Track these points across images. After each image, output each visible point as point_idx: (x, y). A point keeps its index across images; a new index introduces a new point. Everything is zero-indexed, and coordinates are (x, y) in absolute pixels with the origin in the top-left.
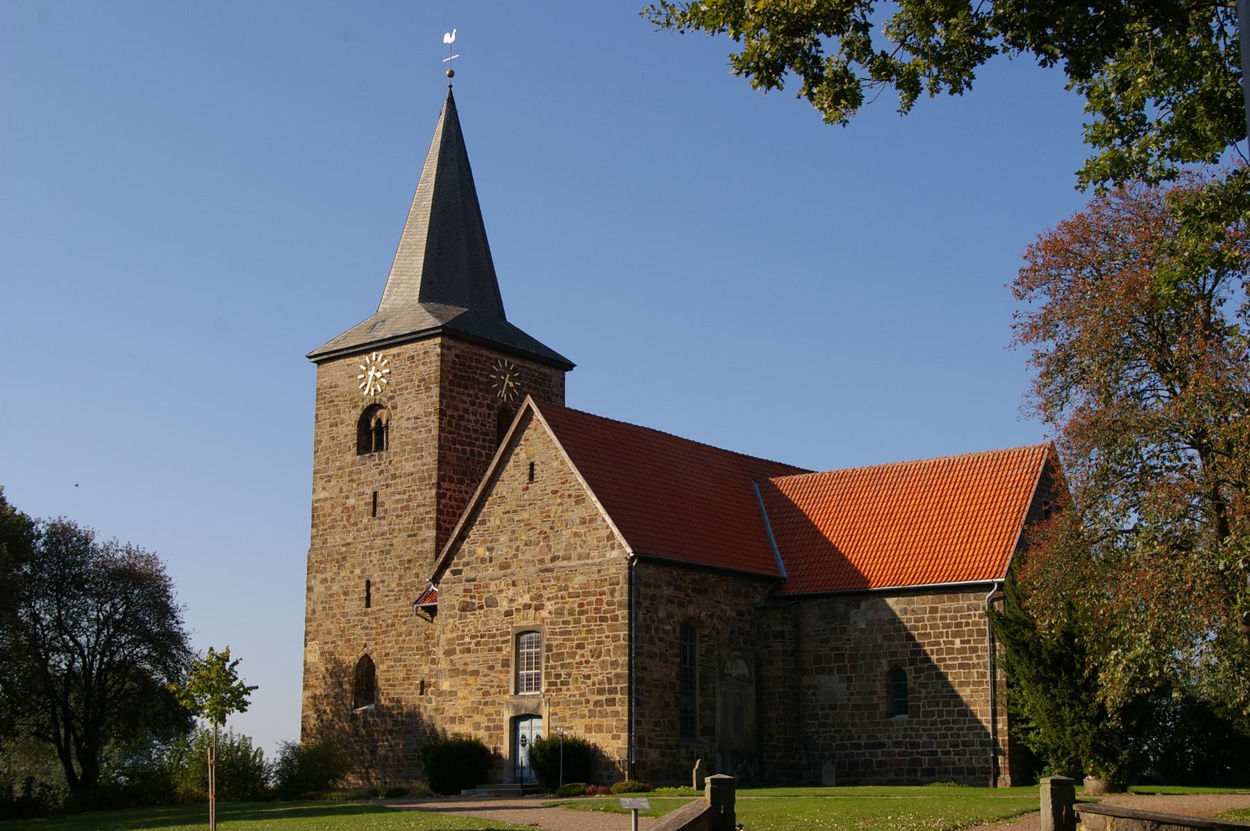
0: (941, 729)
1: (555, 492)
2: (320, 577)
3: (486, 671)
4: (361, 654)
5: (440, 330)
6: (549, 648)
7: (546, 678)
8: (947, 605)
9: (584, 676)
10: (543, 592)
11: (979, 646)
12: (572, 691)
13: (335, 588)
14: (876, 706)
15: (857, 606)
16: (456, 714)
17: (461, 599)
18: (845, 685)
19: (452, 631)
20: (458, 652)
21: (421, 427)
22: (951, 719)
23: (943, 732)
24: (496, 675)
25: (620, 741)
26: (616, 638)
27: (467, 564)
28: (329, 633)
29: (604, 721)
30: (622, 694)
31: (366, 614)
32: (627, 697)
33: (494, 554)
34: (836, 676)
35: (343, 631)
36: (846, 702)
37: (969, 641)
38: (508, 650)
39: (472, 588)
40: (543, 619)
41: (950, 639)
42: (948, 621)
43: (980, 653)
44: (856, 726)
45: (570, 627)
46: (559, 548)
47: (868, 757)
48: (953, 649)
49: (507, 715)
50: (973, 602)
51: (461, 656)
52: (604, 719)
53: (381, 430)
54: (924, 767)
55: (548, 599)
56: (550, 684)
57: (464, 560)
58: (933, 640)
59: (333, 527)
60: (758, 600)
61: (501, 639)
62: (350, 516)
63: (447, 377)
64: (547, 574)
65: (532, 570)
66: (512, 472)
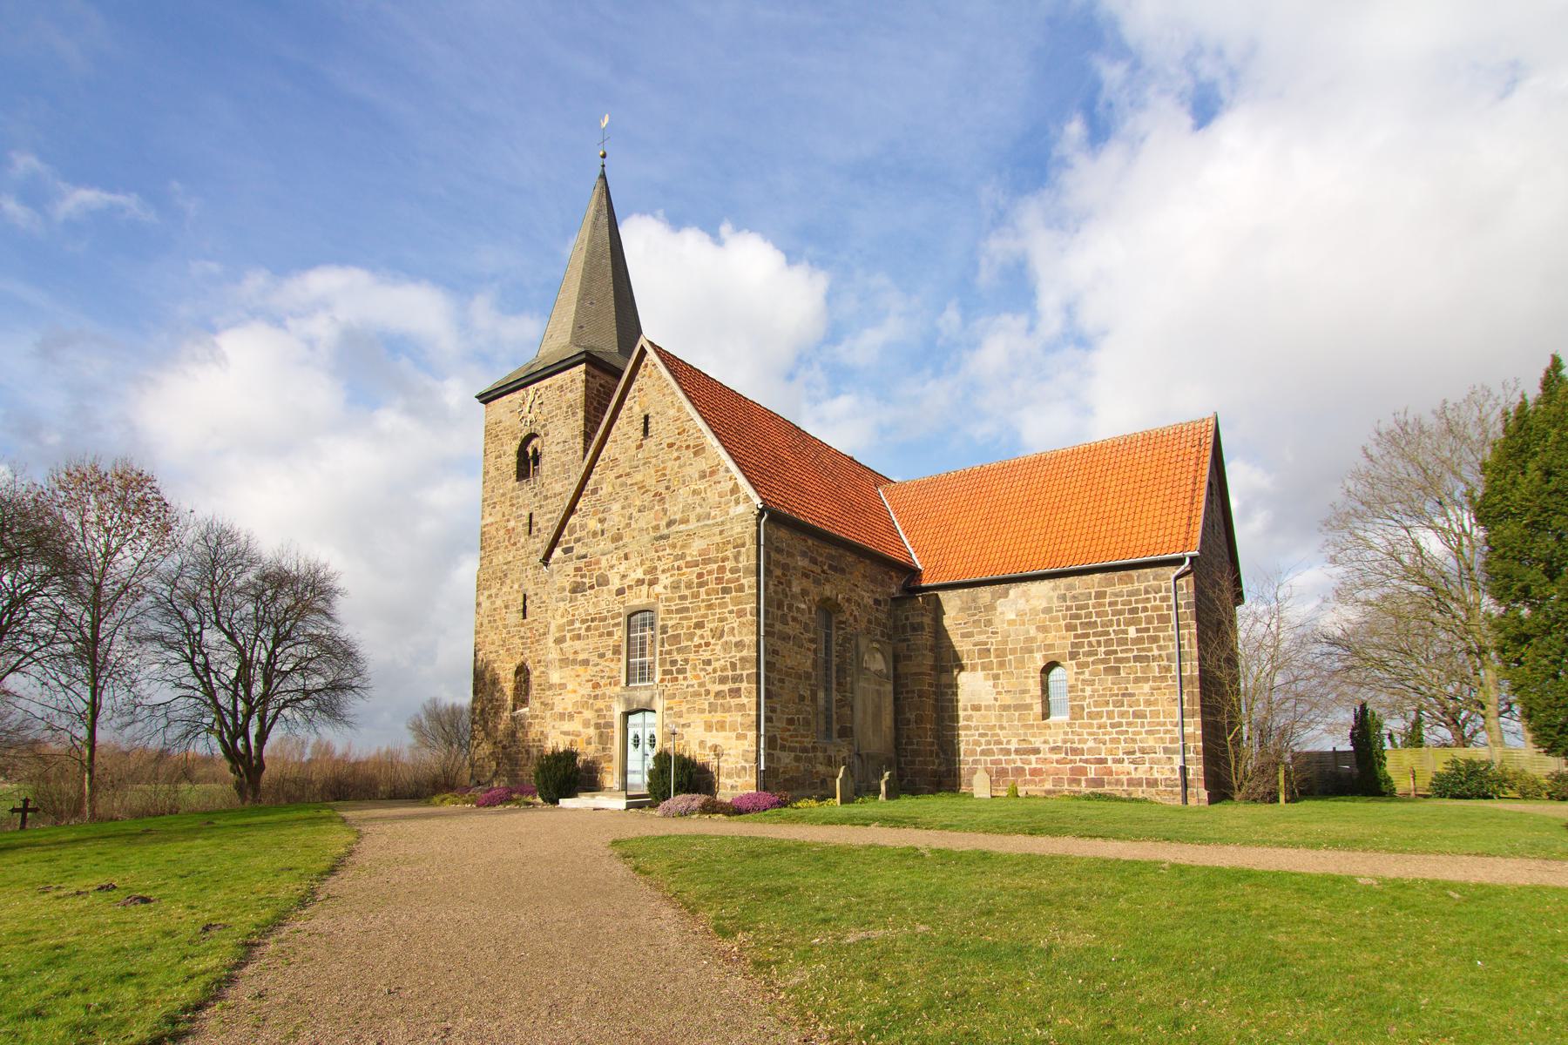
0: (1111, 733)
1: (671, 445)
2: (486, 593)
3: (596, 659)
4: (518, 662)
5: (583, 356)
6: (664, 631)
7: (661, 665)
8: (1118, 588)
9: (703, 661)
10: (657, 563)
11: (1161, 634)
12: (691, 679)
13: (499, 603)
14: (1028, 707)
15: (1006, 595)
16: (565, 709)
17: (573, 579)
18: (991, 683)
19: (562, 616)
20: (568, 639)
21: (569, 449)
22: (1124, 721)
23: (1115, 736)
24: (607, 664)
25: (746, 743)
26: (741, 614)
27: (578, 540)
28: (493, 644)
29: (728, 718)
30: (748, 682)
31: (522, 625)
32: (754, 686)
33: (606, 525)
34: (980, 674)
35: (504, 641)
36: (993, 702)
37: (1147, 630)
38: (620, 634)
39: (583, 565)
40: (657, 597)
41: (1122, 627)
42: (1119, 607)
43: (1162, 643)
44: (1005, 728)
45: (687, 603)
46: (675, 512)
47: (1019, 764)
48: (1127, 639)
49: (618, 709)
50: (1152, 582)
51: (572, 643)
52: (726, 714)
53: (537, 458)
54: (1090, 776)
55: (663, 571)
56: (665, 672)
57: (575, 536)
58: (1100, 629)
59: (498, 548)
60: (894, 590)
61: (612, 622)
62: (510, 537)
63: (592, 403)
64: (662, 542)
65: (646, 538)
66: (624, 430)
